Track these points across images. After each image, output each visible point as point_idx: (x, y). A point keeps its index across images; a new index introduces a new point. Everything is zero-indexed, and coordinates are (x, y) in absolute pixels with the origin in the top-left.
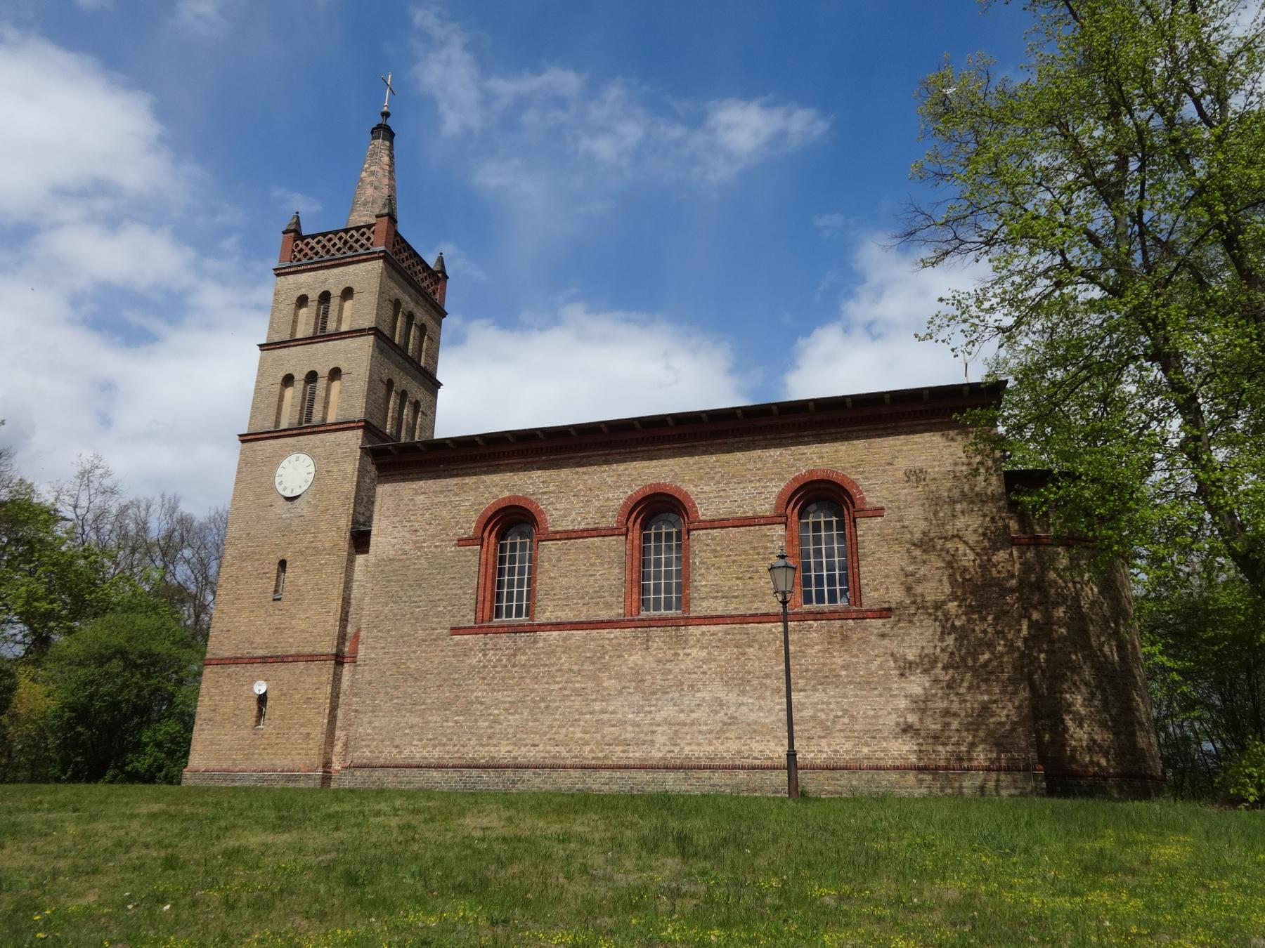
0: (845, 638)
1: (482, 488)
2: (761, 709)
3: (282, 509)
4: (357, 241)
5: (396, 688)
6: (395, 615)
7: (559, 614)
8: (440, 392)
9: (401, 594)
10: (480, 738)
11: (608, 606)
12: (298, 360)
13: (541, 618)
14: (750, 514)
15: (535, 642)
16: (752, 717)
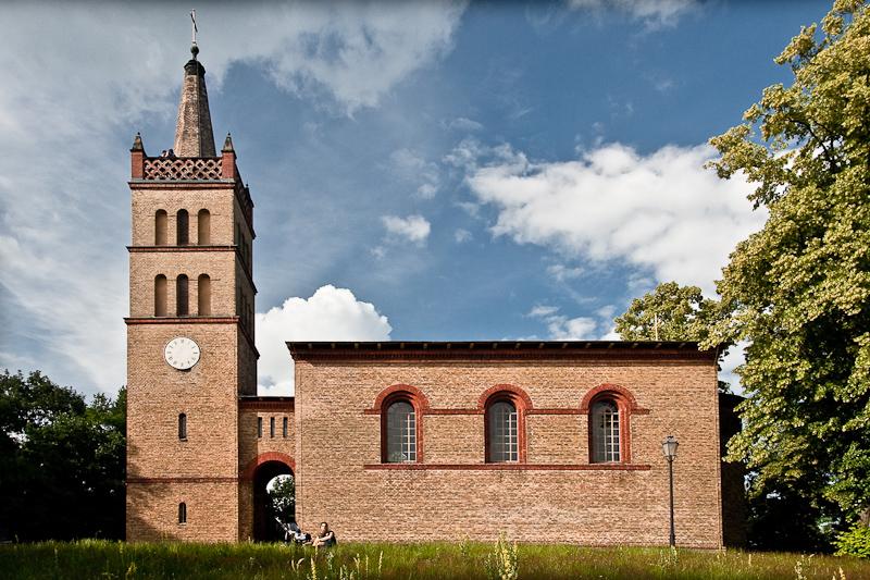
0: (622, 480)
1: (378, 378)
2: (571, 516)
3: (173, 377)
4: (205, 170)
5: (328, 500)
6: (321, 456)
7: (441, 460)
8: (302, 300)
9: (324, 442)
10: (391, 530)
11: (474, 456)
12: (171, 264)
13: (636, 461)
14: (566, 407)
15: (425, 475)
16: (566, 520)
